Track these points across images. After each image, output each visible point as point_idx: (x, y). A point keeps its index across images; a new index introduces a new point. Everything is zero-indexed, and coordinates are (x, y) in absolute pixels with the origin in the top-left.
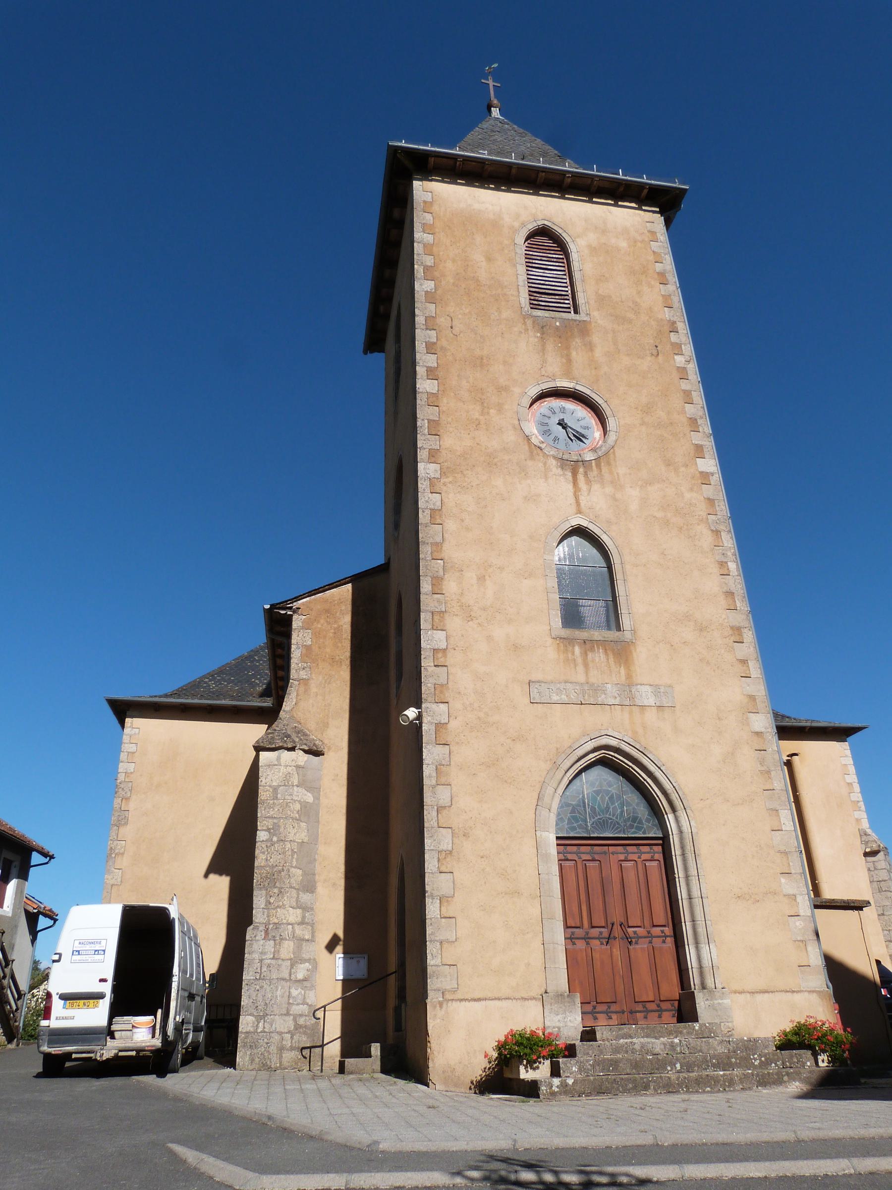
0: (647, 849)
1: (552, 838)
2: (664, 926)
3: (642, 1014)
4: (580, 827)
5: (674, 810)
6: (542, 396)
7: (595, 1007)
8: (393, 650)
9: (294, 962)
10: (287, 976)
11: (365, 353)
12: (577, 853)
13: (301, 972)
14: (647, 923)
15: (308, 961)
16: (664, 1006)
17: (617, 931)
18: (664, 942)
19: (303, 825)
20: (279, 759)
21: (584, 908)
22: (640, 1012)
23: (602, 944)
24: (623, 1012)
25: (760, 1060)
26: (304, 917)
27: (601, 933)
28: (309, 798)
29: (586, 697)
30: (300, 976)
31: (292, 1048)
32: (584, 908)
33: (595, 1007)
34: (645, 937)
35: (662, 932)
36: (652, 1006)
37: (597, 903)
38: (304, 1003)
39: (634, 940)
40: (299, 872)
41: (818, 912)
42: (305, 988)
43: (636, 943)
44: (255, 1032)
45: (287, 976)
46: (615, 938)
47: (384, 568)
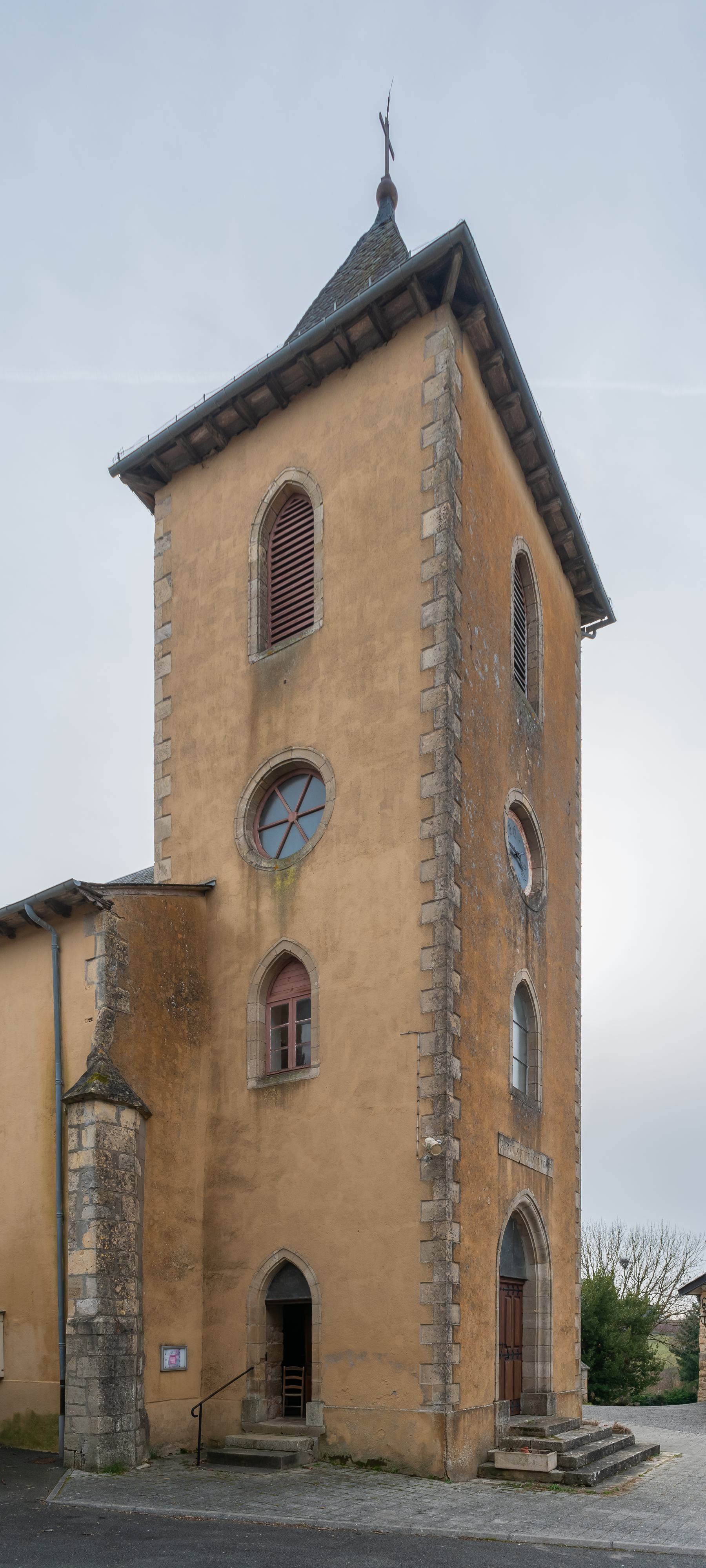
11: (113, 472)
20: (118, 1117)
44: (114, 1432)
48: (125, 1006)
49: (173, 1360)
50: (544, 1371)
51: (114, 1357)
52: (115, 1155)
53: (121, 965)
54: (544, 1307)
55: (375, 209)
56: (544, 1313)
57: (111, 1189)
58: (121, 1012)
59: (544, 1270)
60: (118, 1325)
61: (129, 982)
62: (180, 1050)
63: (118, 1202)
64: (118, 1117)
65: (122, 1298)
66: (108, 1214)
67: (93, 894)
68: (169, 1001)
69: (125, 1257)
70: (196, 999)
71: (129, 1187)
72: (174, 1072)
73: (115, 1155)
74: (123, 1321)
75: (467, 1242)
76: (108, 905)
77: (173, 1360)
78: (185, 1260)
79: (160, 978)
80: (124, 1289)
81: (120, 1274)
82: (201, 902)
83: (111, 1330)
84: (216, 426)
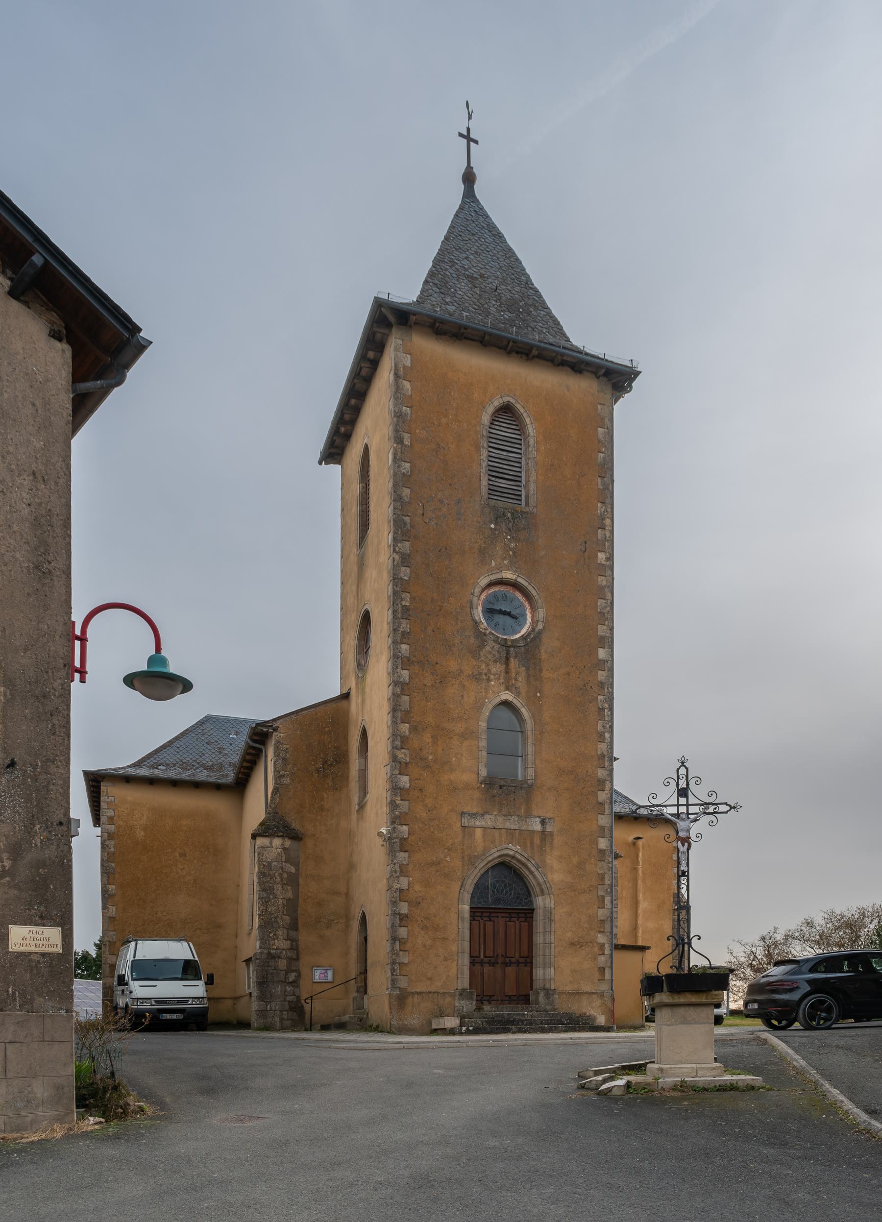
1: (467, 908)
4: (484, 901)
5: (803, 1037)
6: (491, 585)
8: (694, 999)
9: (287, 972)
10: (8, 1046)
11: (320, 463)
13: (292, 977)
14: (517, 955)
15: (295, 971)
17: (500, 960)
19: (289, 888)
20: (271, 843)
21: (482, 946)
26: (292, 945)
28: (293, 870)
30: (291, 980)
31: (288, 1019)
38: (294, 995)
40: (288, 918)
42: (294, 986)
44: (266, 1010)
45: (8, 1046)
47: (346, 696)
48: (286, 781)
49: (322, 976)
50: (544, 974)
51: (266, 971)
52: (269, 864)
53: (284, 759)
54: (545, 928)
55: (462, 187)
56: (545, 932)
57: (267, 882)
58: (284, 784)
59: (544, 900)
60: (269, 954)
61: (289, 766)
62: (325, 796)
63: (272, 889)
64: (271, 843)
65: (274, 939)
66: (265, 895)
67: (266, 727)
68: (318, 770)
69: (276, 918)
70: (338, 762)
71: (278, 879)
72: (322, 809)
73: (269, 864)
74: (273, 951)
75: (417, 888)
76: (275, 730)
77: (322, 976)
78: (332, 918)
79: (311, 758)
80: (275, 935)
81: (272, 926)
82: (344, 703)
83: (265, 956)
84: (78, 638)
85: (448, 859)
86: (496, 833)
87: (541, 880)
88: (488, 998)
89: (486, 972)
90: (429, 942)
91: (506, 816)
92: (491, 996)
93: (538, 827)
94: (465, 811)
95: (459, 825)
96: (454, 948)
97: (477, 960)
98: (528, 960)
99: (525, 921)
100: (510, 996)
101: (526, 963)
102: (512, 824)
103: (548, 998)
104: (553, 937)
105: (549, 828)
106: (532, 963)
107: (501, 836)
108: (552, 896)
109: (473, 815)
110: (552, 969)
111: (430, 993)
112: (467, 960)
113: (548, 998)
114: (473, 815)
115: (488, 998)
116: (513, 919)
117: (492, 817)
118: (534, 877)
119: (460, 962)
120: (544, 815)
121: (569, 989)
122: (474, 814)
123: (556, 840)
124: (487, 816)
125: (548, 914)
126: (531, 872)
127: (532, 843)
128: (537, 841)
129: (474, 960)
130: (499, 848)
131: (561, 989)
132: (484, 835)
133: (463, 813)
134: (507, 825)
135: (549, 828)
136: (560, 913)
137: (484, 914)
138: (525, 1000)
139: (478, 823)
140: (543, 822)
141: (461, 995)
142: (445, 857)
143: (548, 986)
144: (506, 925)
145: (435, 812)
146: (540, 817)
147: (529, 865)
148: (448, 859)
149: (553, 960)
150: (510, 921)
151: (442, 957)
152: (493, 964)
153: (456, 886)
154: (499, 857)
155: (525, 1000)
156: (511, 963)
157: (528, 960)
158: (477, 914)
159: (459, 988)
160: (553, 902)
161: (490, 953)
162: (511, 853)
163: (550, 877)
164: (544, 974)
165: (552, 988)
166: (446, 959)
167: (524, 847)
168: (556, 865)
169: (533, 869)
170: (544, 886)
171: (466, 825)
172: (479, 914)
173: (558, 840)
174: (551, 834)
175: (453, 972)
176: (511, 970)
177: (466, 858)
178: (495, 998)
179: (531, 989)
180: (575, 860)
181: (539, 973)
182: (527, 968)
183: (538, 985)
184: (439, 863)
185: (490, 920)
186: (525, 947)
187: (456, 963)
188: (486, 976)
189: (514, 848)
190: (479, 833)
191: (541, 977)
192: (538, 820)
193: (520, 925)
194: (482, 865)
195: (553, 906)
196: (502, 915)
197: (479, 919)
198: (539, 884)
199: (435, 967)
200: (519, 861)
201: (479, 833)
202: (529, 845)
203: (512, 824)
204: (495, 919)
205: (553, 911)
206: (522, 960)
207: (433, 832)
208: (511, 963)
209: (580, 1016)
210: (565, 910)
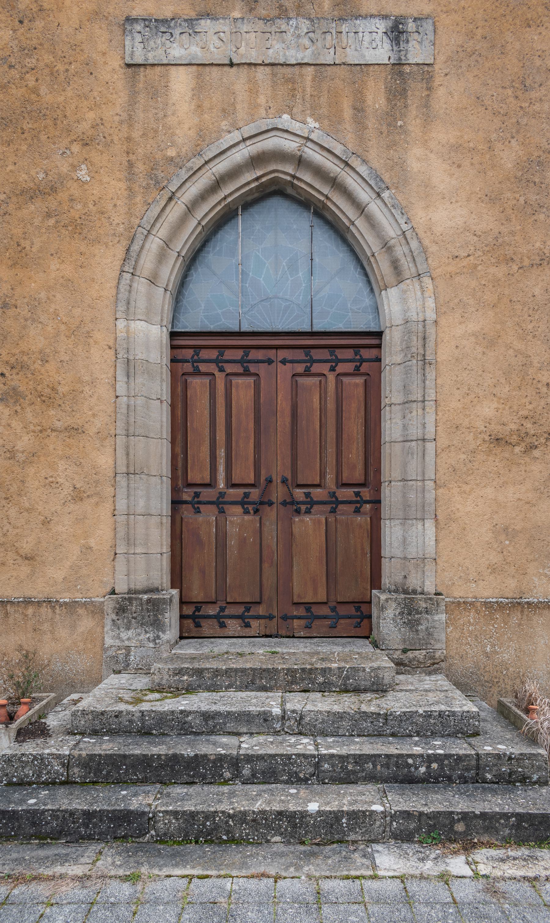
0: (349, 354)
2: (253, 486)
3: (303, 622)
7: (222, 609)
12: (216, 361)
14: (330, 478)
16: (343, 610)
17: (278, 493)
18: (357, 511)
21: (221, 453)
22: (299, 618)
23: (247, 512)
24: (270, 617)
25: (428, 767)
27: (246, 495)
29: (242, 50)
32: (221, 453)
33: (222, 609)
34: (350, 502)
35: (357, 494)
36: (325, 611)
37: (246, 447)
39: (303, 508)
41: (373, 328)
43: (308, 512)
46: (270, 504)
50: (404, 542)
59: (404, 300)
85: (83, 174)
86: (238, 79)
87: (391, 232)
88: (240, 610)
89: (232, 530)
90: (25, 442)
91: (266, 20)
92: (248, 606)
93: (381, 52)
94: (134, 14)
95: (115, 63)
96: (104, 460)
97: (207, 494)
98: (366, 493)
99: (357, 372)
100: (308, 606)
101: (357, 504)
102: (291, 44)
103: (412, 625)
104: (430, 419)
105: (417, 52)
106: (377, 502)
107: (253, 91)
108: (427, 281)
109: (160, 25)
110: (430, 524)
111: (28, 602)
112: (155, 496)
113: (412, 625)
114: (160, 25)
115: (240, 610)
116: (316, 368)
117: (223, 26)
118: (370, 220)
119: (122, 505)
120: (396, 11)
121: (488, 590)
122: (165, 21)
123: (441, 92)
124: (205, 24)
125: (416, 343)
126: (361, 208)
127: (359, 109)
128: (376, 98)
129: (185, 495)
130: (248, 131)
131: (460, 592)
132: (199, 88)
133: (129, 20)
134: (277, 51)
135: (417, 52)
136: (455, 338)
137: (229, 354)
138: (358, 621)
139: (177, 52)
140: (397, 33)
141: (121, 610)
142: (74, 167)
143: (413, 582)
144: (295, 388)
145: (39, 24)
146: (385, 17)
147: (351, 181)
148: (83, 174)
149: (430, 496)
150: (307, 373)
151: (67, 490)
152: (257, 507)
153: (107, 260)
154: (256, 160)
155: (358, 621)
156: (311, 503)
157: (363, 492)
158: (205, 354)
159: (121, 587)
160: (430, 303)
161: (244, 472)
162: (290, 145)
163: (420, 216)
164: (404, 542)
165: (430, 588)
166: (78, 496)
167: (332, 123)
168: (440, 175)
169: (363, 195)
170: (400, 251)
171: (139, 59)
172: (213, 354)
173: (449, 92)
174: (426, 69)
175: (102, 535)
176: (309, 527)
177: (140, 168)
178: (261, 610)
179: (376, 581)
180: (509, 156)
181: (392, 534)
182: (362, 520)
183: (390, 573)
184: (54, 190)
185: (247, 373)
186: (354, 454)
187: (108, 506)
188: (232, 542)
189: (296, 126)
190: (181, 82)
191: (398, 553)
192: (381, 26)
193: (339, 384)
194: (193, 190)
195: (431, 315)
196: (283, 354)
197: (212, 368)
198: (387, 247)
199: (46, 522)
200: (319, 172)
201: (181, 82)
202: (348, 113)
203: (291, 44)
204: (262, 369)
205: (431, 330)
206: (347, 493)
207: (35, 91)
208: (311, 503)
209: (135, 853)
210: (472, 327)
